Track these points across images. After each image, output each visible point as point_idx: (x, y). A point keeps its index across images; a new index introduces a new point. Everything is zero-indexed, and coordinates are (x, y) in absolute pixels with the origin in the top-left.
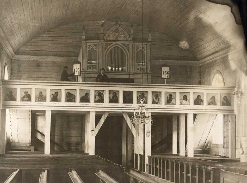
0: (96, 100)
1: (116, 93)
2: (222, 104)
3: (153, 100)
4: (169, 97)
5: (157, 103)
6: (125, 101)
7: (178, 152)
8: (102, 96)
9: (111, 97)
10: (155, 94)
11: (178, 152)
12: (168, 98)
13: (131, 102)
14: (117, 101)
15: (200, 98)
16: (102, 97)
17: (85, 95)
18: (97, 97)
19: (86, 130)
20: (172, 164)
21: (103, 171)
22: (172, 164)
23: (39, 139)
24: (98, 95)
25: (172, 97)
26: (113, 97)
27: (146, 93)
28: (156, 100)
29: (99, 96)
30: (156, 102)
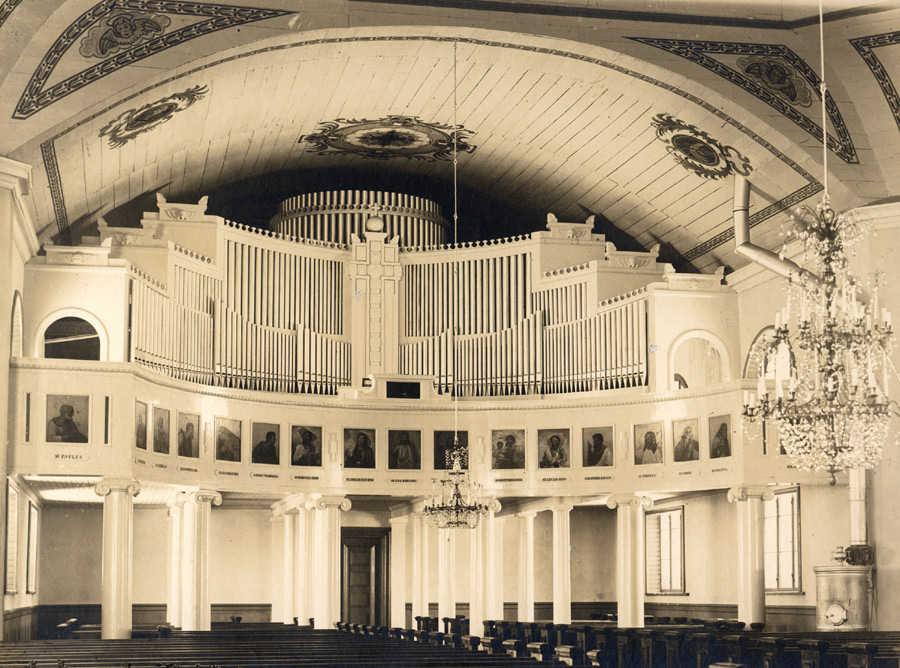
0: (297, 458)
1: (366, 437)
2: (52, 432)
3: (543, 455)
4: (595, 442)
5: (556, 465)
6: (395, 462)
7: (397, 196)
8: (315, 443)
9: (351, 450)
10: (549, 437)
11: (397, 196)
12: (590, 446)
13: (415, 463)
14: (370, 463)
15: (58, 418)
16: (312, 448)
17: (265, 440)
18: (298, 447)
19: (631, 10)
20: (337, 240)
21: (85, 235)
22: (337, 240)
23: (537, 230)
24: (301, 440)
25: (601, 443)
26: (355, 451)
27: (520, 435)
28: (553, 455)
29: (304, 443)
30: (554, 460)
